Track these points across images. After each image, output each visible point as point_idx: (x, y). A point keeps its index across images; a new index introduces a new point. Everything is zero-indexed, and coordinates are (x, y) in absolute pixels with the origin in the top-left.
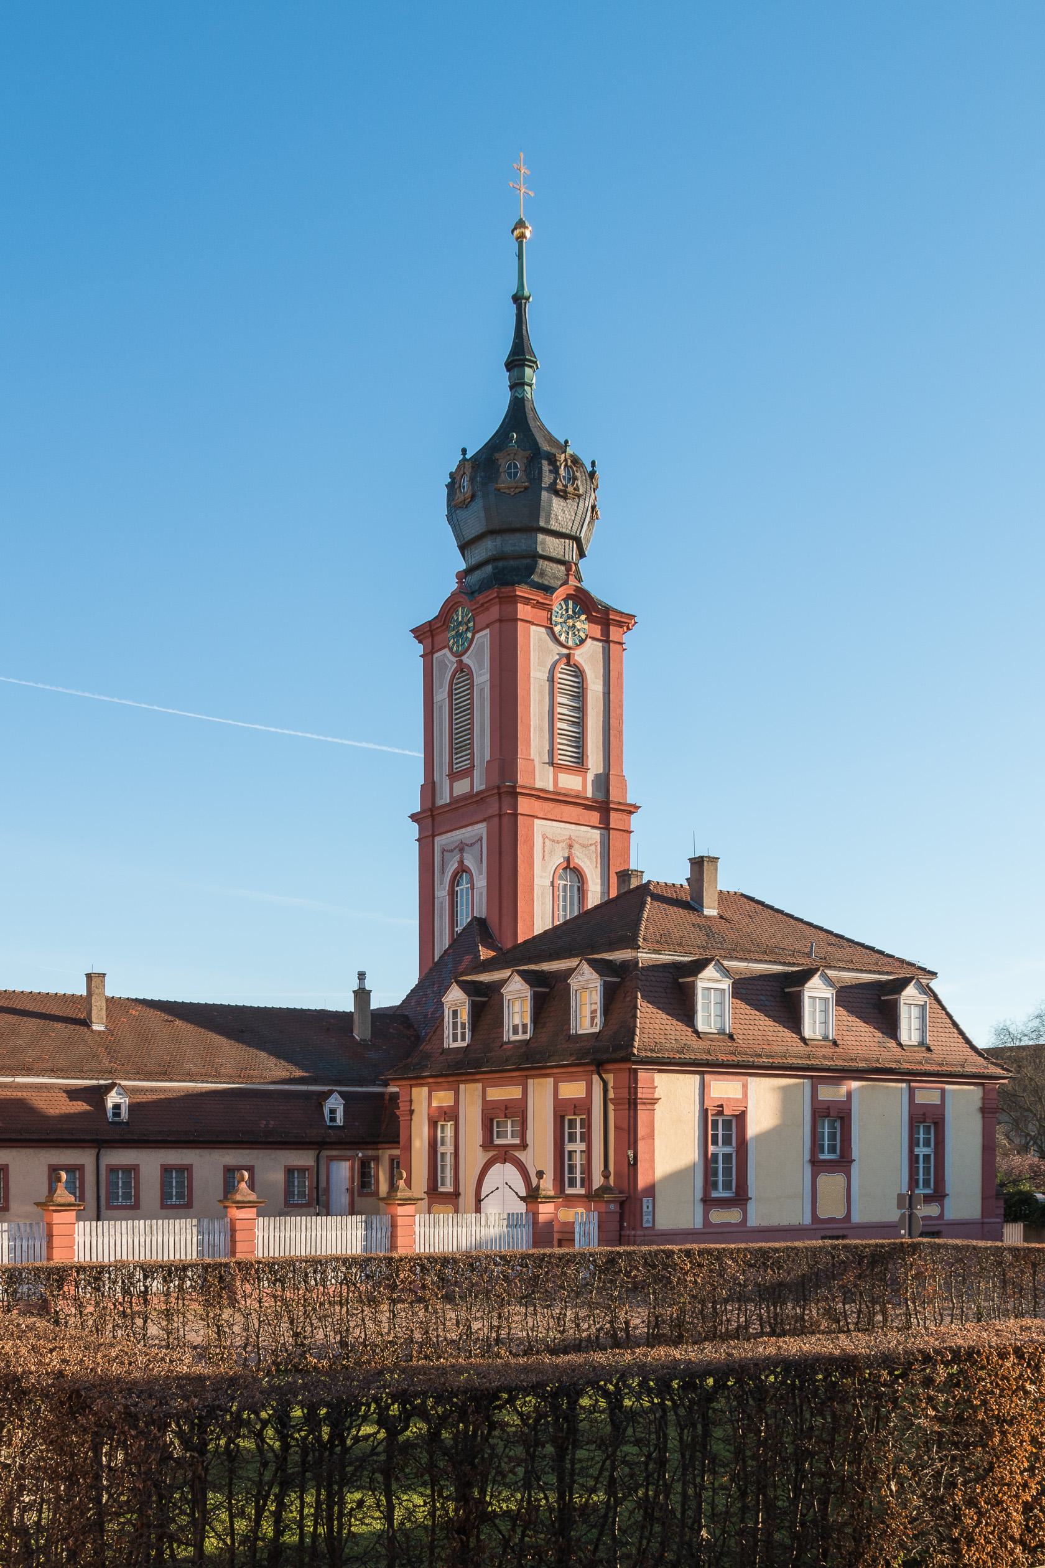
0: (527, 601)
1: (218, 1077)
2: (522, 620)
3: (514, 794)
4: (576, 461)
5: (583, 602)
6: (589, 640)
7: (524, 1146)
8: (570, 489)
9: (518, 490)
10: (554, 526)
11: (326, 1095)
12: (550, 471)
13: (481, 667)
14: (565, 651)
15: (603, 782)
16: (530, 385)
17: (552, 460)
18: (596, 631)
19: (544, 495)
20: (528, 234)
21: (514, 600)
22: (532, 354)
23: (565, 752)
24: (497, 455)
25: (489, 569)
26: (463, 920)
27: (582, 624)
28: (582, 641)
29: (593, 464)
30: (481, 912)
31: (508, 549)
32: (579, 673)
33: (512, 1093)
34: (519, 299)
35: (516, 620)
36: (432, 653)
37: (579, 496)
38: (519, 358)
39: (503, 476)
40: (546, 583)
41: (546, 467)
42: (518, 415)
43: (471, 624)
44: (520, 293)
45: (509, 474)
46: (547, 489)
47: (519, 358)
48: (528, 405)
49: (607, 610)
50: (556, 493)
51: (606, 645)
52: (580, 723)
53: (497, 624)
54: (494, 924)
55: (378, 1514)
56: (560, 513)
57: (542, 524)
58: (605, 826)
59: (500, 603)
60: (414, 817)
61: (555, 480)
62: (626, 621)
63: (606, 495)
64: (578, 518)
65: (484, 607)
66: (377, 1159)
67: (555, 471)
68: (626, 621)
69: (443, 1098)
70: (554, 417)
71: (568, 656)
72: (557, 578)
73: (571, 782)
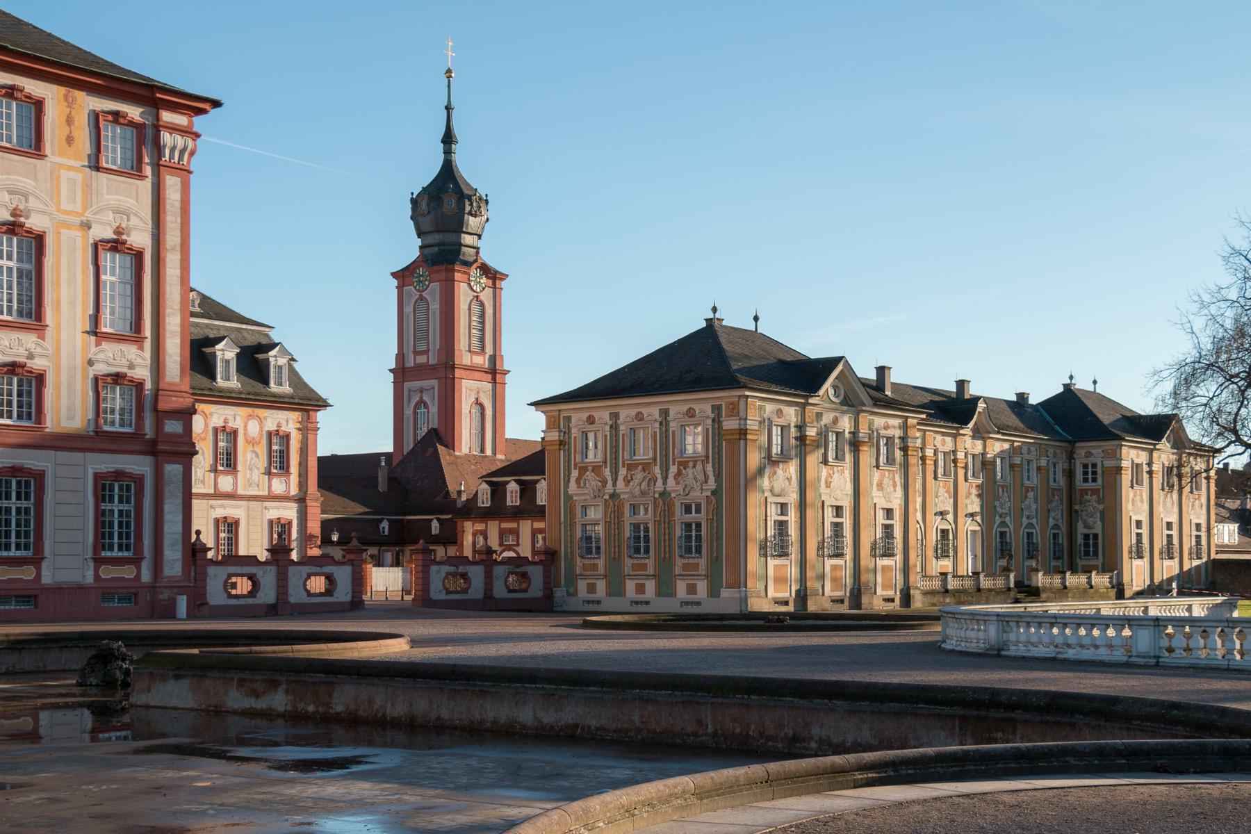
1: (335, 512)
3: (453, 367)
4: (480, 199)
5: (486, 270)
7: (518, 545)
11: (381, 521)
15: (493, 359)
21: (454, 271)
22: (482, 192)
23: (476, 344)
25: (436, 249)
26: (423, 431)
27: (484, 280)
30: (436, 426)
32: (482, 304)
33: (514, 525)
34: (448, 108)
35: (454, 280)
38: (448, 139)
42: (448, 172)
47: (448, 139)
49: (496, 272)
52: (482, 330)
54: (442, 432)
56: (472, 222)
58: (494, 381)
63: (492, 211)
66: (402, 551)
67: (471, 204)
69: (480, 526)
70: (469, 171)
73: (479, 360)
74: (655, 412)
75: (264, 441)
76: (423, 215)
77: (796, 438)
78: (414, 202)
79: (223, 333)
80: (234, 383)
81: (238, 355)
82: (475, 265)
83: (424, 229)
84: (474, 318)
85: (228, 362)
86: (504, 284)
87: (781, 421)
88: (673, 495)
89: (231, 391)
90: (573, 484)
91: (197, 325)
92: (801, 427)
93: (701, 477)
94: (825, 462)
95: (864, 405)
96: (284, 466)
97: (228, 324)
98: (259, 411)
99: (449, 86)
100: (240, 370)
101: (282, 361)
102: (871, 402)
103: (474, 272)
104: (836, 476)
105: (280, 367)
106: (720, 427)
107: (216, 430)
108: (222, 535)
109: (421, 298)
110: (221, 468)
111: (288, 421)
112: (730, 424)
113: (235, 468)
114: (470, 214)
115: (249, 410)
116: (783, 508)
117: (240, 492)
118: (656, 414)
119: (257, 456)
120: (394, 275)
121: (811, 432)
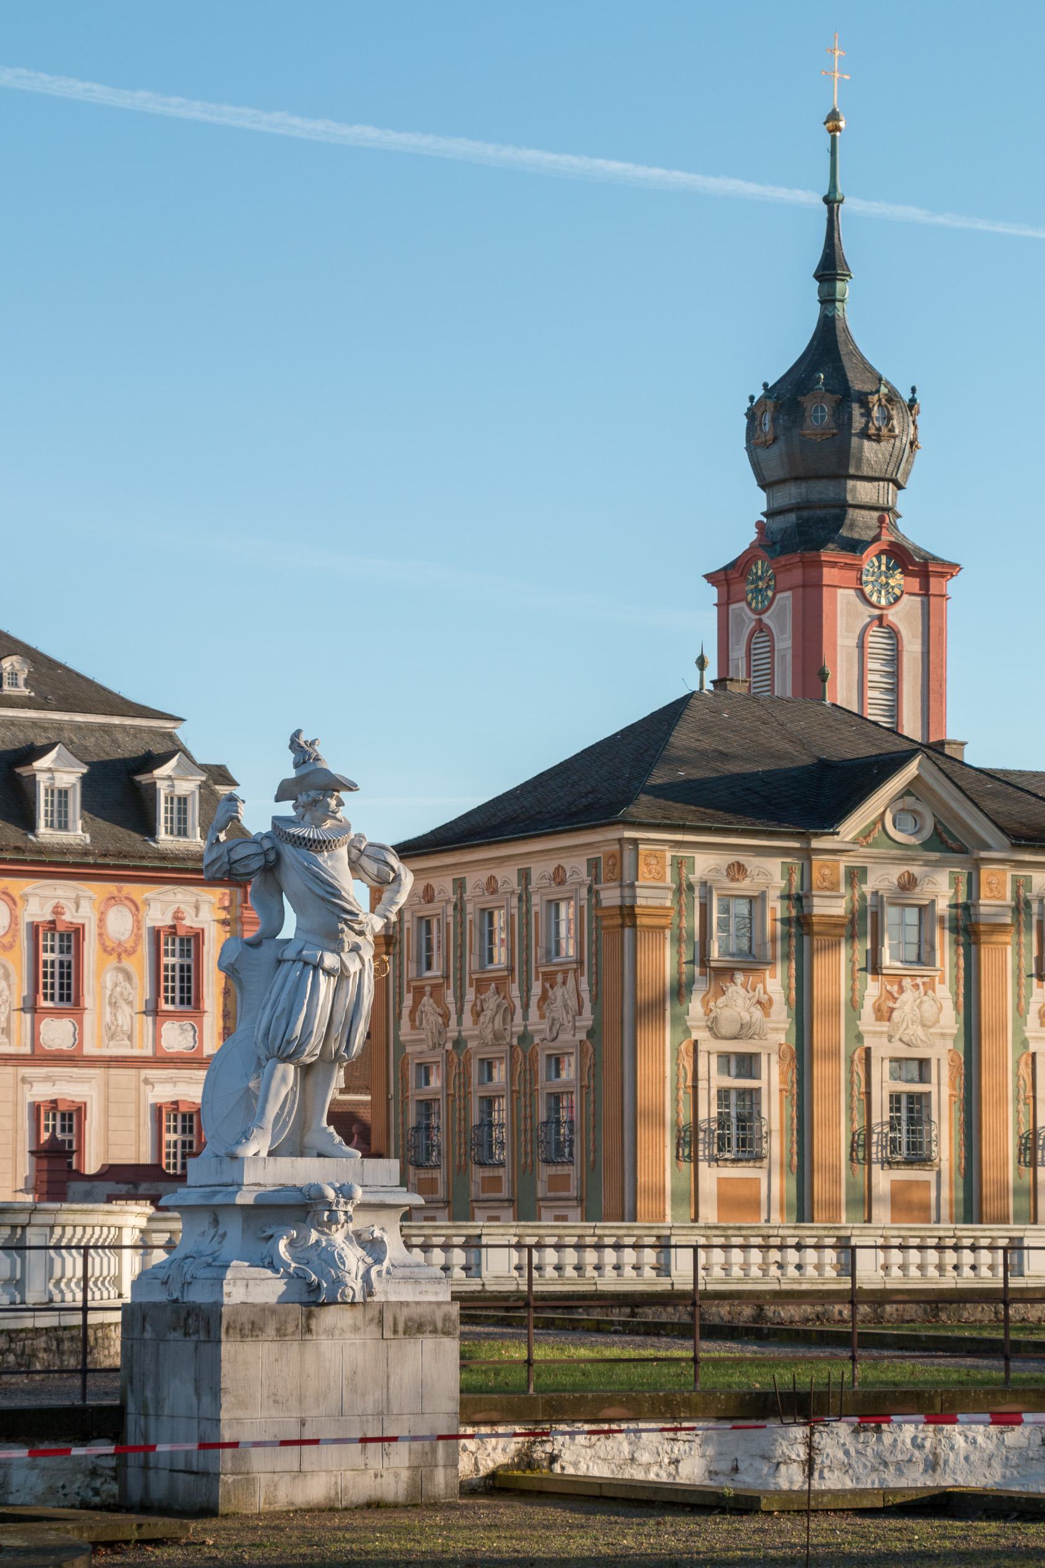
0: (833, 565)
2: (828, 586)
5: (901, 557)
6: (905, 597)
8: (884, 431)
9: (824, 437)
10: (866, 471)
12: (862, 415)
13: (783, 631)
14: (877, 612)
16: (842, 301)
17: (863, 399)
18: (914, 583)
19: (855, 441)
20: (842, 124)
21: (819, 564)
24: (801, 399)
25: (792, 517)
27: (897, 579)
28: (897, 599)
29: (913, 390)
31: (814, 496)
32: (893, 634)
36: (728, 604)
37: (895, 437)
38: (830, 269)
39: (809, 421)
40: (856, 536)
41: (856, 410)
42: (828, 345)
43: (772, 583)
44: (831, 197)
45: (816, 418)
46: (857, 435)
47: (830, 269)
48: (839, 325)
50: (869, 437)
51: (925, 599)
53: (801, 589)
55: (760, 986)
57: (852, 471)
59: (804, 567)
60: (765, 385)
61: (867, 423)
62: (950, 569)
64: (894, 459)
65: (787, 568)
67: (868, 414)
68: (950, 569)
70: (879, 341)
71: (880, 618)
72: (868, 528)
74: (507, 876)
75: (145, 949)
76: (766, 446)
77: (786, 921)
78: (752, 415)
79: (52, 736)
80: (77, 834)
81: (85, 780)
82: (873, 549)
83: (771, 476)
84: (871, 665)
85: (64, 793)
86: (952, 586)
87: (745, 886)
88: (537, 1040)
89: (64, 850)
90: (467, 1017)
91: (12, 722)
92: (798, 899)
93: (573, 1003)
94: (874, 967)
95: (987, 847)
96: (188, 995)
97: (79, 718)
98: (129, 888)
99: (833, 152)
100: (87, 805)
101: (188, 786)
102: (1006, 841)
103: (870, 561)
104: (908, 996)
105: (183, 800)
106: (598, 901)
107: (34, 928)
108: (169, 1137)
109: (760, 627)
110: (170, 1007)
111: (204, 909)
112: (610, 897)
113: (77, 1003)
114: (865, 434)
115: (111, 887)
116: (747, 1064)
117: (90, 1049)
118: (514, 879)
119: (128, 977)
120: (711, 578)
121: (830, 906)
